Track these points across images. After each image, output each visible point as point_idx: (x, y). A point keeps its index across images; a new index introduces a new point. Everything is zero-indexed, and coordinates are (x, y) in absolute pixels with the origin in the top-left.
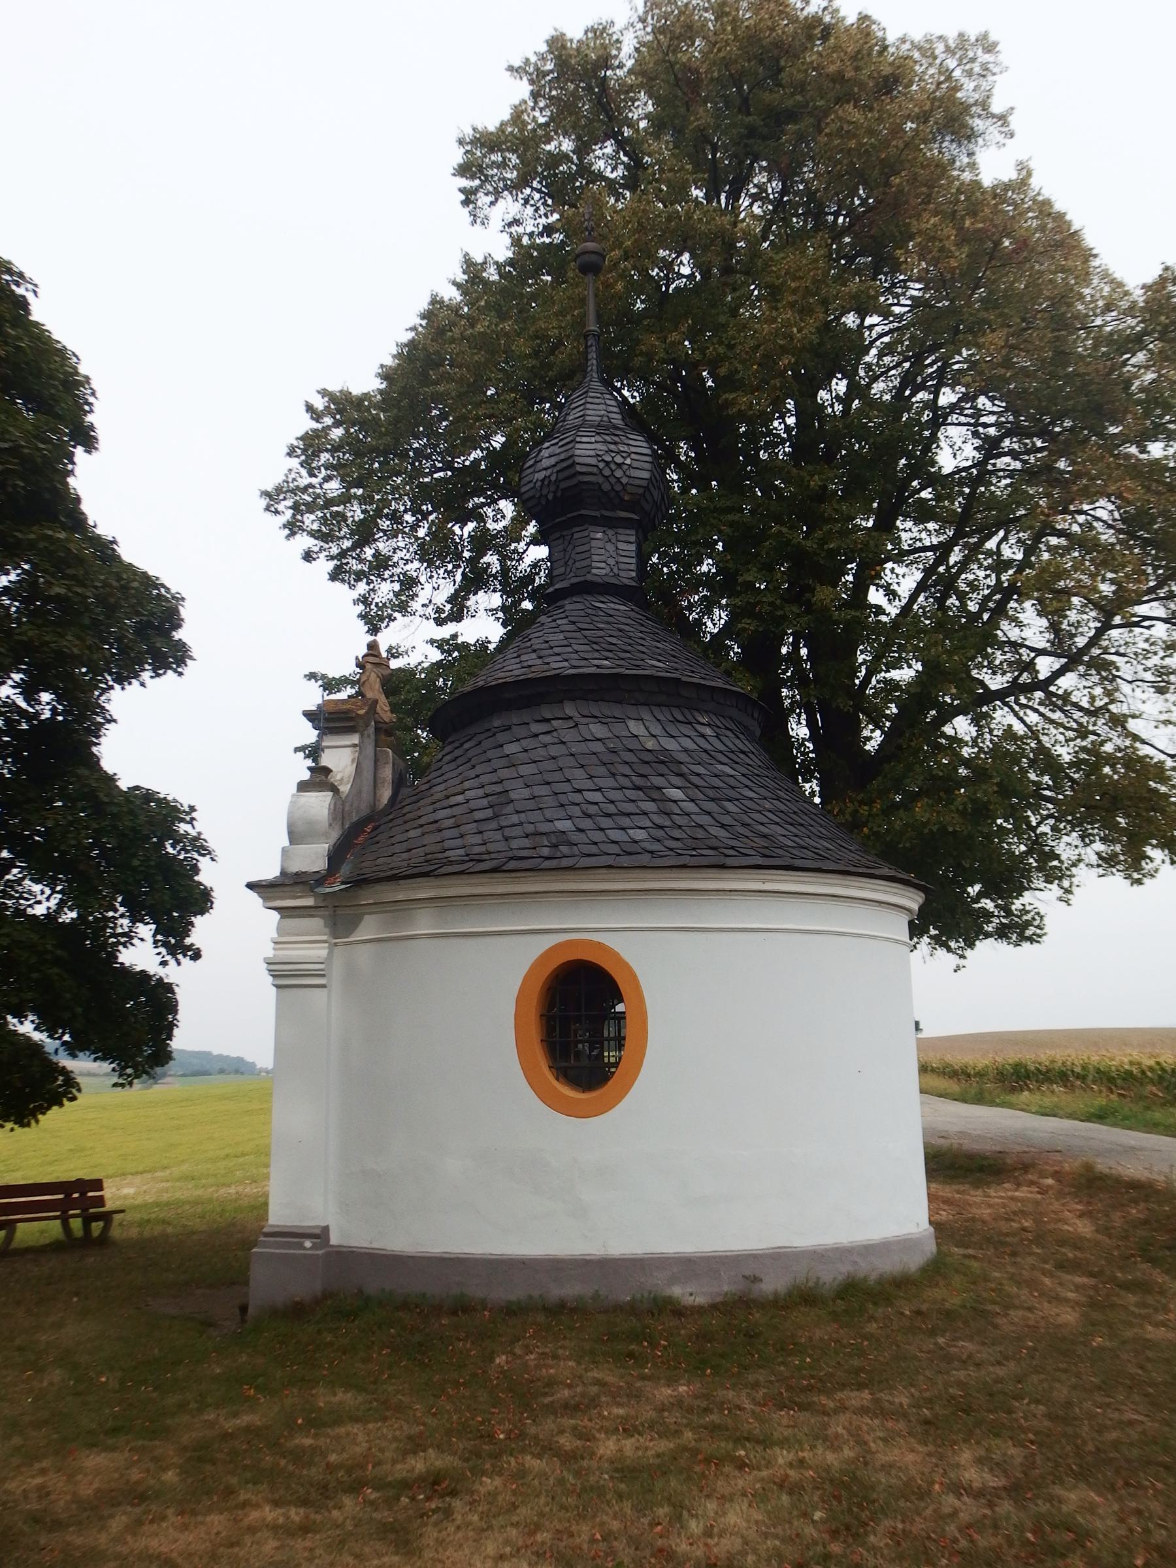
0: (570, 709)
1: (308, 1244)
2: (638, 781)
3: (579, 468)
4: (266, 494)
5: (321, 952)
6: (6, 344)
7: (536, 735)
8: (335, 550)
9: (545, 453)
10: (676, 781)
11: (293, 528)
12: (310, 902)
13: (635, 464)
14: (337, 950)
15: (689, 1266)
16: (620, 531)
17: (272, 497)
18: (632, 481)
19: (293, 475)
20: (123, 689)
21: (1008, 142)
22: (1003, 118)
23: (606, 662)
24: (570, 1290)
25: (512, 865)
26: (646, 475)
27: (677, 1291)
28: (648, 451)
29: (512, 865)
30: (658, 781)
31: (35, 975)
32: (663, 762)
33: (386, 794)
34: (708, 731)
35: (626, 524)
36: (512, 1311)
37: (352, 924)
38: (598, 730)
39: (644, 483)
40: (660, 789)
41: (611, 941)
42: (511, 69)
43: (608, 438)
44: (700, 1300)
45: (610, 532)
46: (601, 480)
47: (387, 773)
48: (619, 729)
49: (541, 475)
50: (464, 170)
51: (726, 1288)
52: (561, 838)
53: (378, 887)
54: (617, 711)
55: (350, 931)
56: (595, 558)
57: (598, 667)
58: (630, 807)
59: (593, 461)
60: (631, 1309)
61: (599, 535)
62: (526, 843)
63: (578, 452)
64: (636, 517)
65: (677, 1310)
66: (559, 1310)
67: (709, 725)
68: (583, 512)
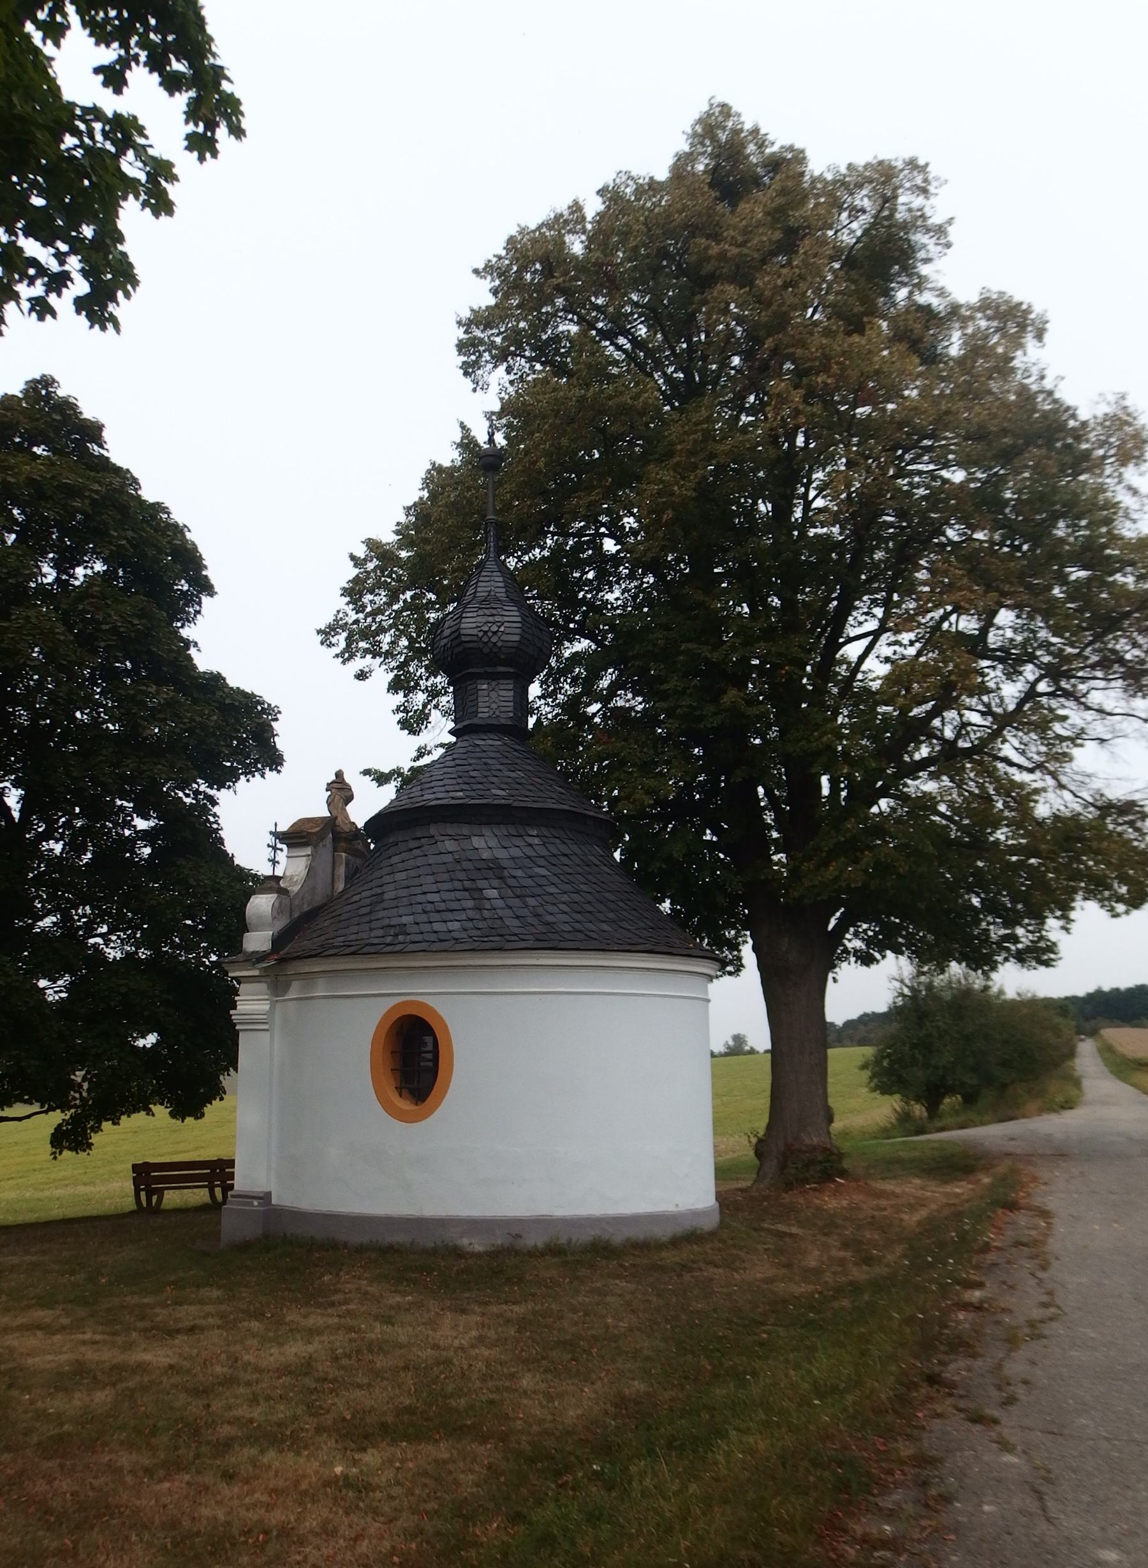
0: (433, 830)
1: (256, 1203)
2: (467, 884)
3: (464, 638)
4: (319, 632)
5: (265, 1007)
6: (111, 543)
7: (411, 850)
8: (394, 664)
9: (446, 625)
10: (496, 883)
11: (347, 655)
12: (256, 973)
13: (508, 631)
14: (278, 1005)
15: (475, 1225)
16: (501, 681)
17: (327, 634)
18: (506, 644)
19: (341, 615)
20: (248, 780)
21: (948, 251)
22: (940, 231)
23: (461, 794)
24: (400, 1238)
25: (367, 949)
26: (517, 638)
27: (465, 1242)
28: (519, 619)
29: (367, 949)
30: (481, 884)
31: (146, 1013)
32: (491, 868)
33: (340, 886)
34: (536, 841)
35: (505, 676)
36: (361, 1249)
37: (286, 988)
38: (450, 845)
39: (515, 644)
40: (481, 890)
41: (430, 1001)
42: (476, 272)
43: (487, 612)
44: (478, 1248)
45: (494, 683)
46: (481, 645)
47: (341, 871)
48: (465, 844)
49: (445, 641)
50: (461, 347)
51: (499, 1242)
52: (402, 929)
53: (295, 963)
54: (465, 830)
55: (285, 993)
56: (480, 704)
57: (453, 798)
58: (455, 905)
59: (475, 632)
60: (434, 1252)
61: (485, 687)
62: (380, 933)
63: (463, 626)
64: (512, 670)
65: (457, 1253)
66: (388, 1251)
67: (537, 836)
68: (471, 670)
